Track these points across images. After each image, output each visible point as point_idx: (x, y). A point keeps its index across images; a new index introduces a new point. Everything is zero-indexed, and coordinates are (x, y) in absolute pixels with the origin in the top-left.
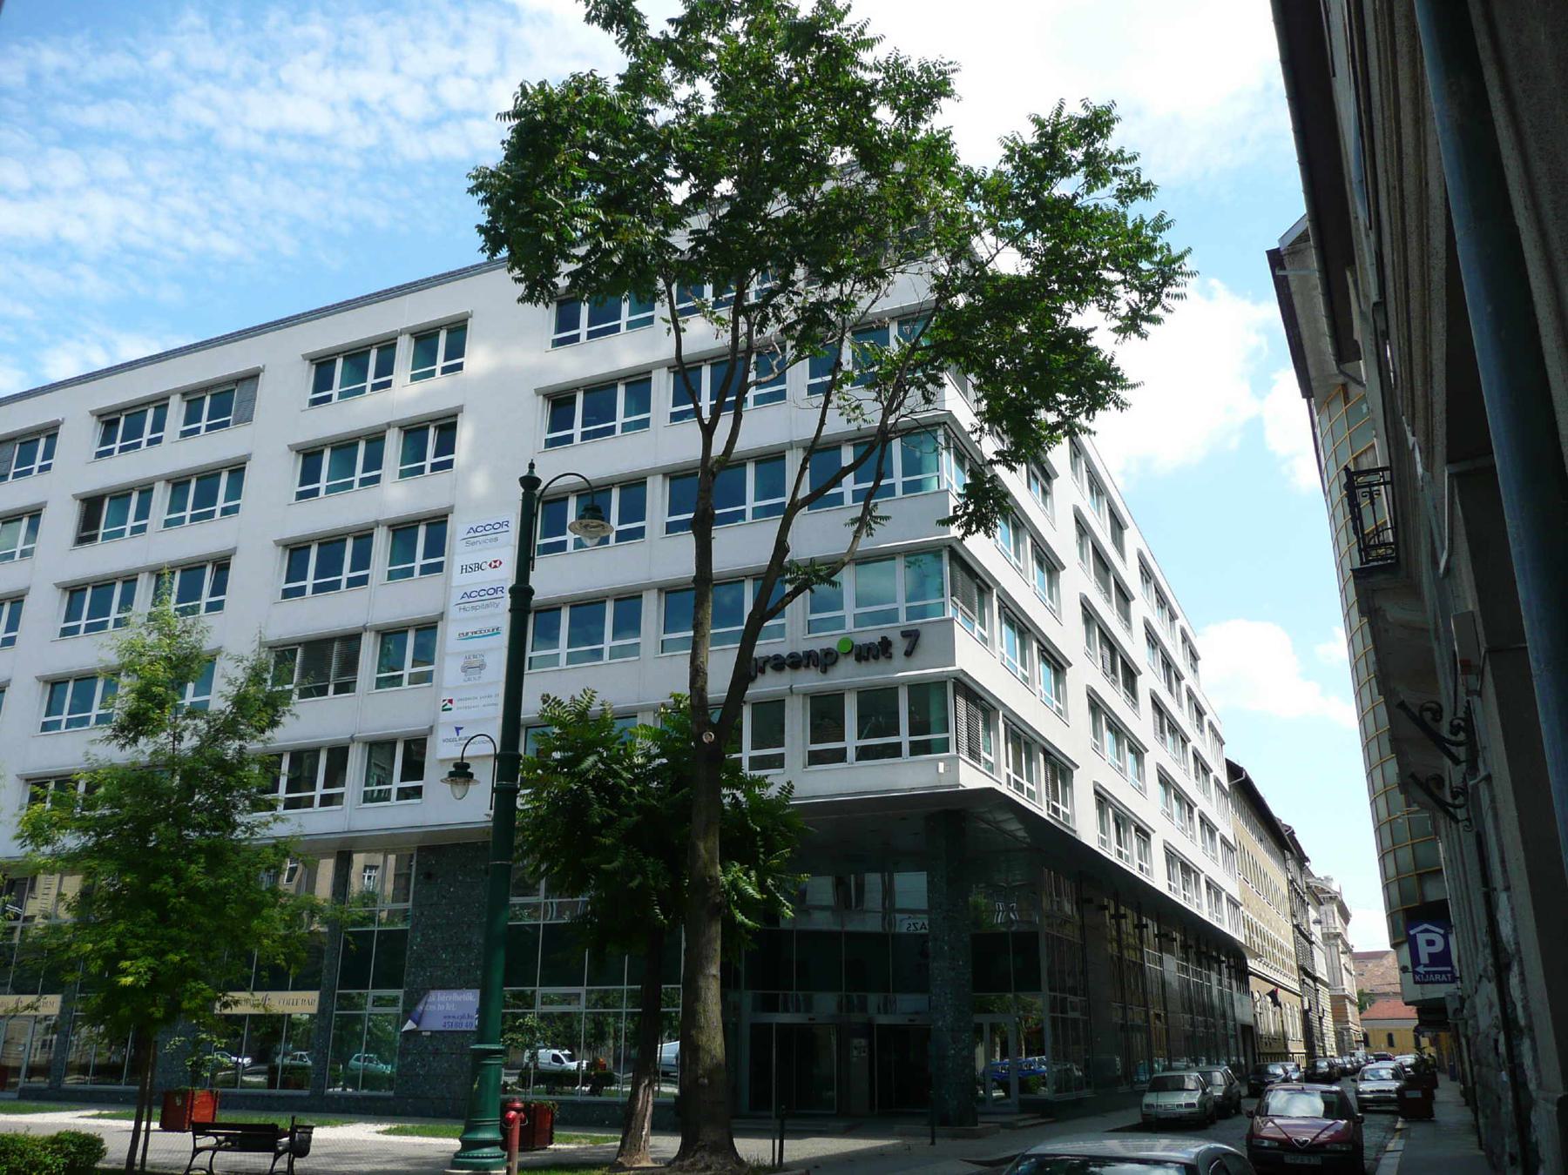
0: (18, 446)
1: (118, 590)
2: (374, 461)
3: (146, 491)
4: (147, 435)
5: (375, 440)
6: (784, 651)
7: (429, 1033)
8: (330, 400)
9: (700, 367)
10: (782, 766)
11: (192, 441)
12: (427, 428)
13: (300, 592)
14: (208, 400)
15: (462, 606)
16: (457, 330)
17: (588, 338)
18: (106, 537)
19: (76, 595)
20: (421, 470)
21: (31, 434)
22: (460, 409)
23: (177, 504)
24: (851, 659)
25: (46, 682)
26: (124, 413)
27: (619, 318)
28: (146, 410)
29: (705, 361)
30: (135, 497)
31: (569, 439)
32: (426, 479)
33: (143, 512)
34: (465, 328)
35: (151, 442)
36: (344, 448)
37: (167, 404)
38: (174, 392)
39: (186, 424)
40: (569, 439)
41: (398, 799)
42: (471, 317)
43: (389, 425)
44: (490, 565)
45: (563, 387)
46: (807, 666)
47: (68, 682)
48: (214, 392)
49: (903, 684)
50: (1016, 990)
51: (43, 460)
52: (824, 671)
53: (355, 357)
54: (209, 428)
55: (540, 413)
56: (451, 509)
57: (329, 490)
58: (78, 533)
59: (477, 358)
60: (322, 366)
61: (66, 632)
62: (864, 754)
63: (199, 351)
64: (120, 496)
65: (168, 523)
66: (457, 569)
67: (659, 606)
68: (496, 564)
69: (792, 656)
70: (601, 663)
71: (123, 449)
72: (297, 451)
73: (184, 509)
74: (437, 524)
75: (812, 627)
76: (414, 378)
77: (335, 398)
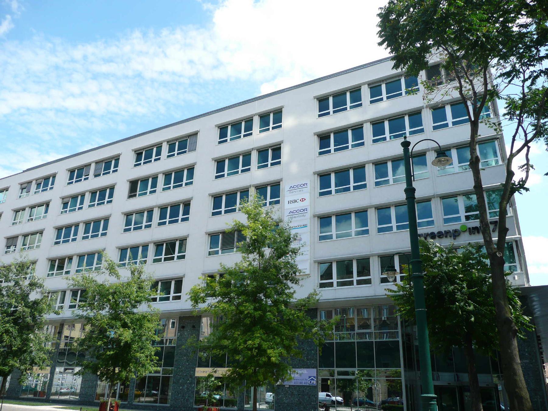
0: (104, 164)
1: (102, 222)
2: (154, 185)
3: (83, 195)
4: (112, 169)
5: (155, 178)
6: (436, 231)
7: (288, 386)
8: (151, 162)
9: (384, 122)
10: (371, 283)
11: (172, 159)
12: (268, 150)
13: (164, 223)
14: (177, 144)
15: (290, 216)
16: (278, 114)
17: (154, 161)
18: (140, 195)
19: (88, 225)
20: (266, 166)
21: (109, 159)
22: (282, 142)
23: (93, 199)
24: (467, 234)
25: (119, 249)
26: (178, 141)
27: (269, 126)
28: (153, 148)
29: (386, 119)
30: (79, 198)
31: (329, 151)
32: (332, 155)
33: (82, 203)
34: (281, 112)
35: (114, 171)
36: (234, 159)
37: (162, 146)
38: (164, 141)
39: (69, 180)
40: (223, 176)
41: (159, 301)
42: (283, 107)
43: (253, 149)
44: (301, 200)
45: (325, 132)
46: (446, 237)
47: (85, 255)
48: (115, 159)
49: (334, 261)
50: (437, 371)
51: (114, 168)
52: (454, 239)
53: (236, 126)
54: (178, 154)
55: (316, 142)
56: (281, 180)
57: (228, 174)
58: (128, 194)
59: (288, 121)
60: (223, 130)
61: (126, 230)
62: (359, 282)
63: (191, 121)
64: (145, 181)
65: (90, 206)
66: (286, 202)
67: (375, 214)
68: (303, 200)
69: (439, 233)
70: (392, 232)
71: (76, 182)
72: (215, 161)
73: (95, 202)
74: (276, 186)
75: (446, 221)
76: (261, 132)
77: (229, 140)
